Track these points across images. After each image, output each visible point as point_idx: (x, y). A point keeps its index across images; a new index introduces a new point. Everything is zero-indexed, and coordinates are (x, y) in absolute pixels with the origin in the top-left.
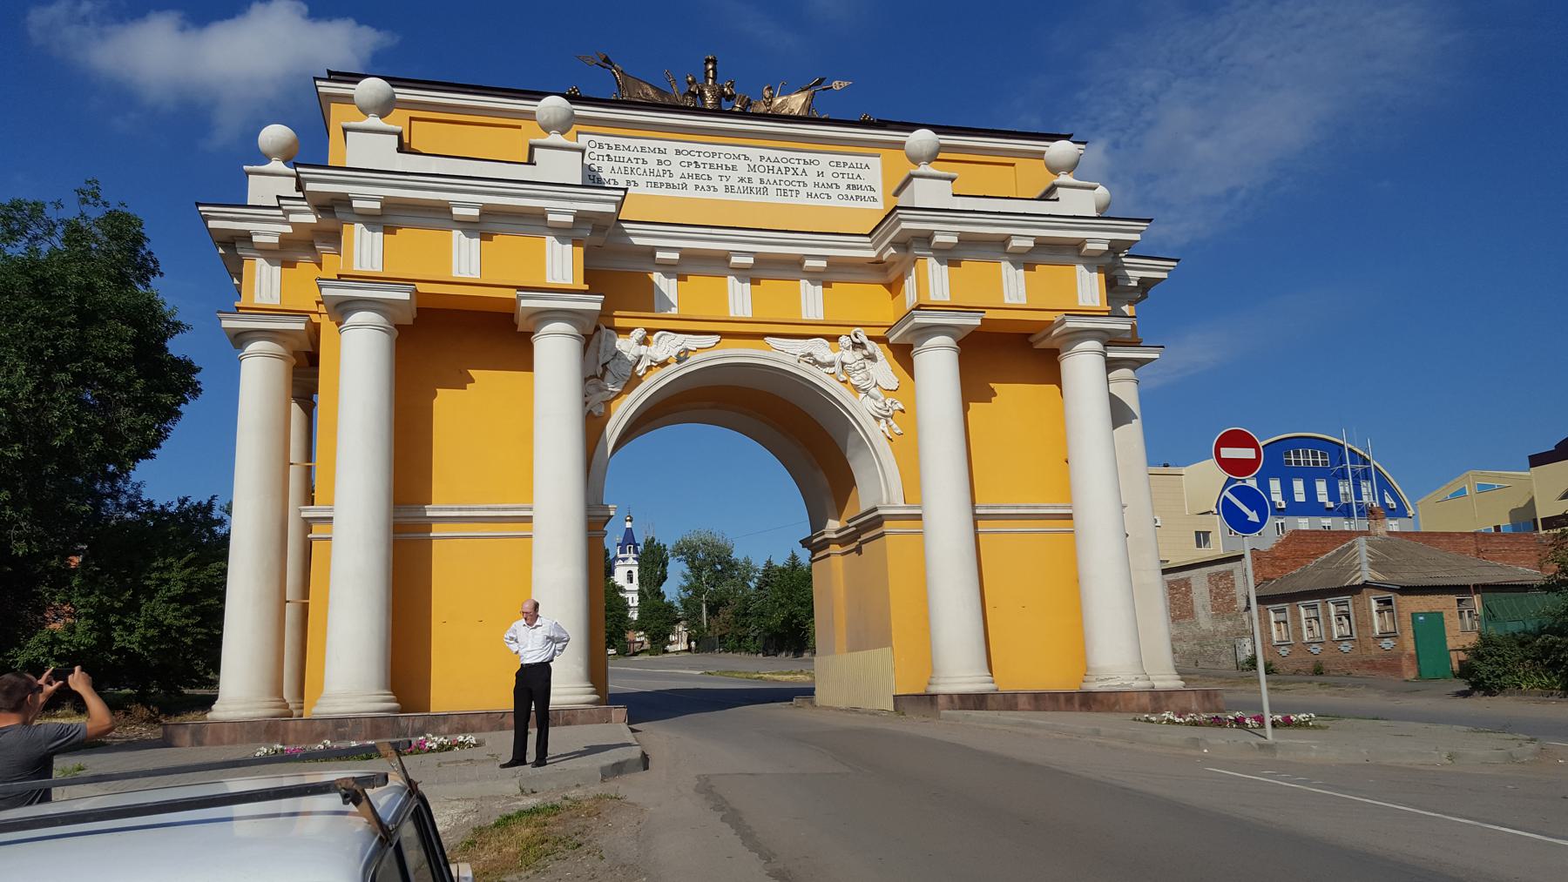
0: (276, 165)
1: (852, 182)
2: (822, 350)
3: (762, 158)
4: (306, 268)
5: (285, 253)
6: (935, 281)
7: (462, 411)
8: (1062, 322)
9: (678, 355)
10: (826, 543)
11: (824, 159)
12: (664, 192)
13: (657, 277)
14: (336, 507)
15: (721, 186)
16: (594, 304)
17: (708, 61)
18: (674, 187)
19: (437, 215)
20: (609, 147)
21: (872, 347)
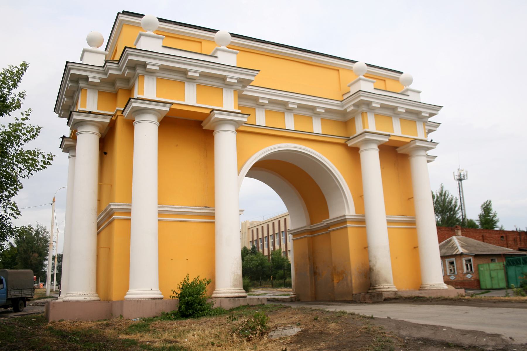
14: (216, 208)
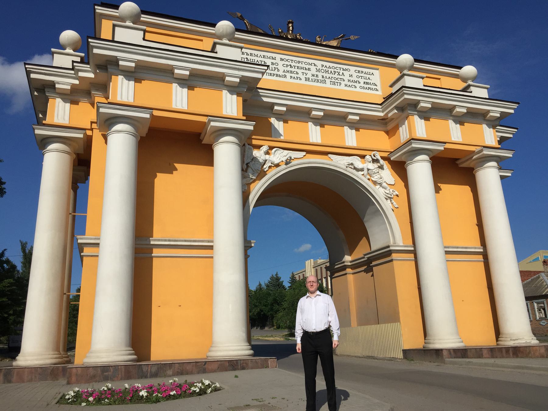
0: (69, 51)
1: (366, 81)
2: (358, 162)
3: (323, 66)
4: (84, 106)
5: (72, 97)
6: (419, 127)
7: (174, 186)
8: (482, 151)
9: (286, 161)
10: (344, 268)
11: (353, 69)
12: (275, 78)
13: (273, 120)
14: (102, 238)
15: (303, 77)
16: (249, 127)
17: (289, 23)
18: (280, 76)
19: (165, 74)
20: (247, 54)
21: (382, 162)
